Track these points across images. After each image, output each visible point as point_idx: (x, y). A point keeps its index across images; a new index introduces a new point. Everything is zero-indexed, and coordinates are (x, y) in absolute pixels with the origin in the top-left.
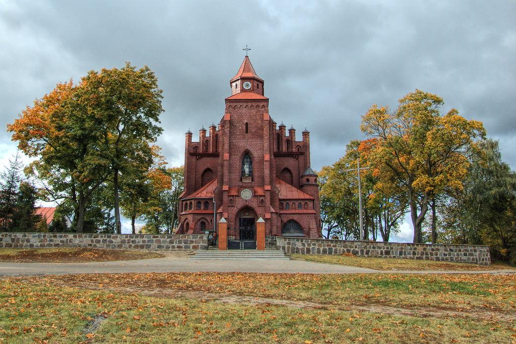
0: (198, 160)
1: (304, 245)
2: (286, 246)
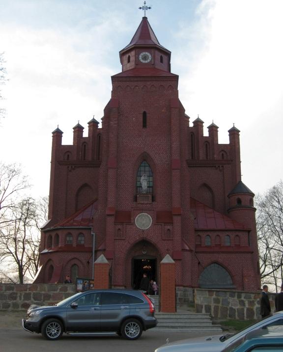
0: (70, 171)
1: (242, 303)
2: (213, 305)
